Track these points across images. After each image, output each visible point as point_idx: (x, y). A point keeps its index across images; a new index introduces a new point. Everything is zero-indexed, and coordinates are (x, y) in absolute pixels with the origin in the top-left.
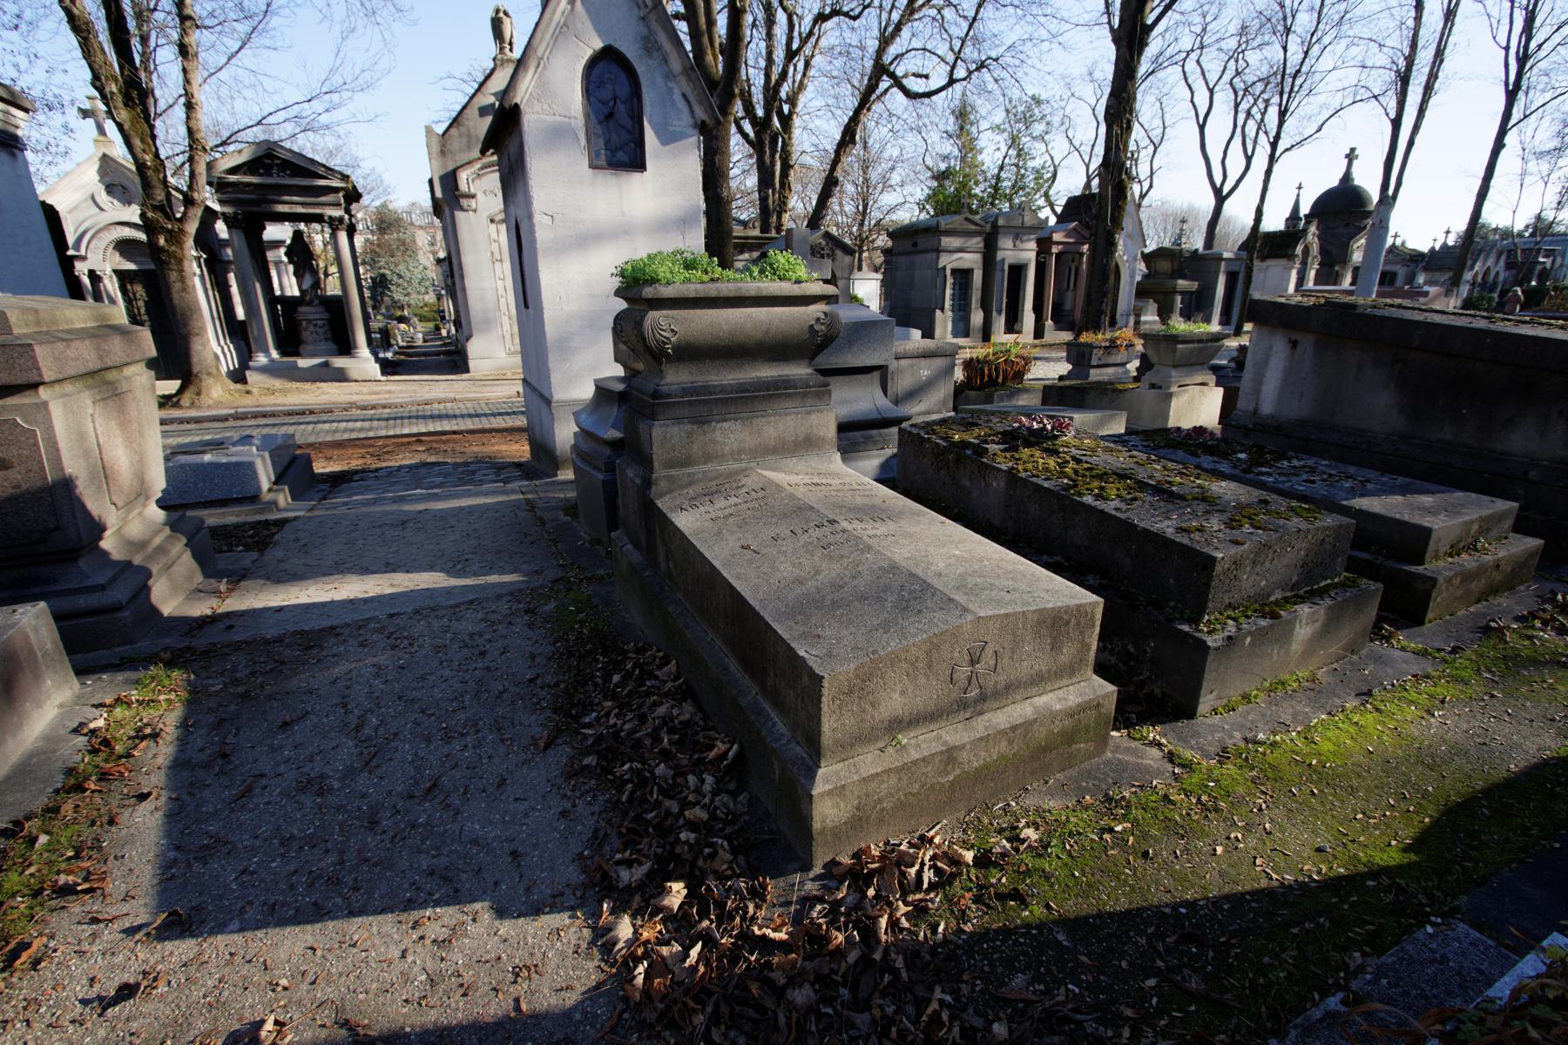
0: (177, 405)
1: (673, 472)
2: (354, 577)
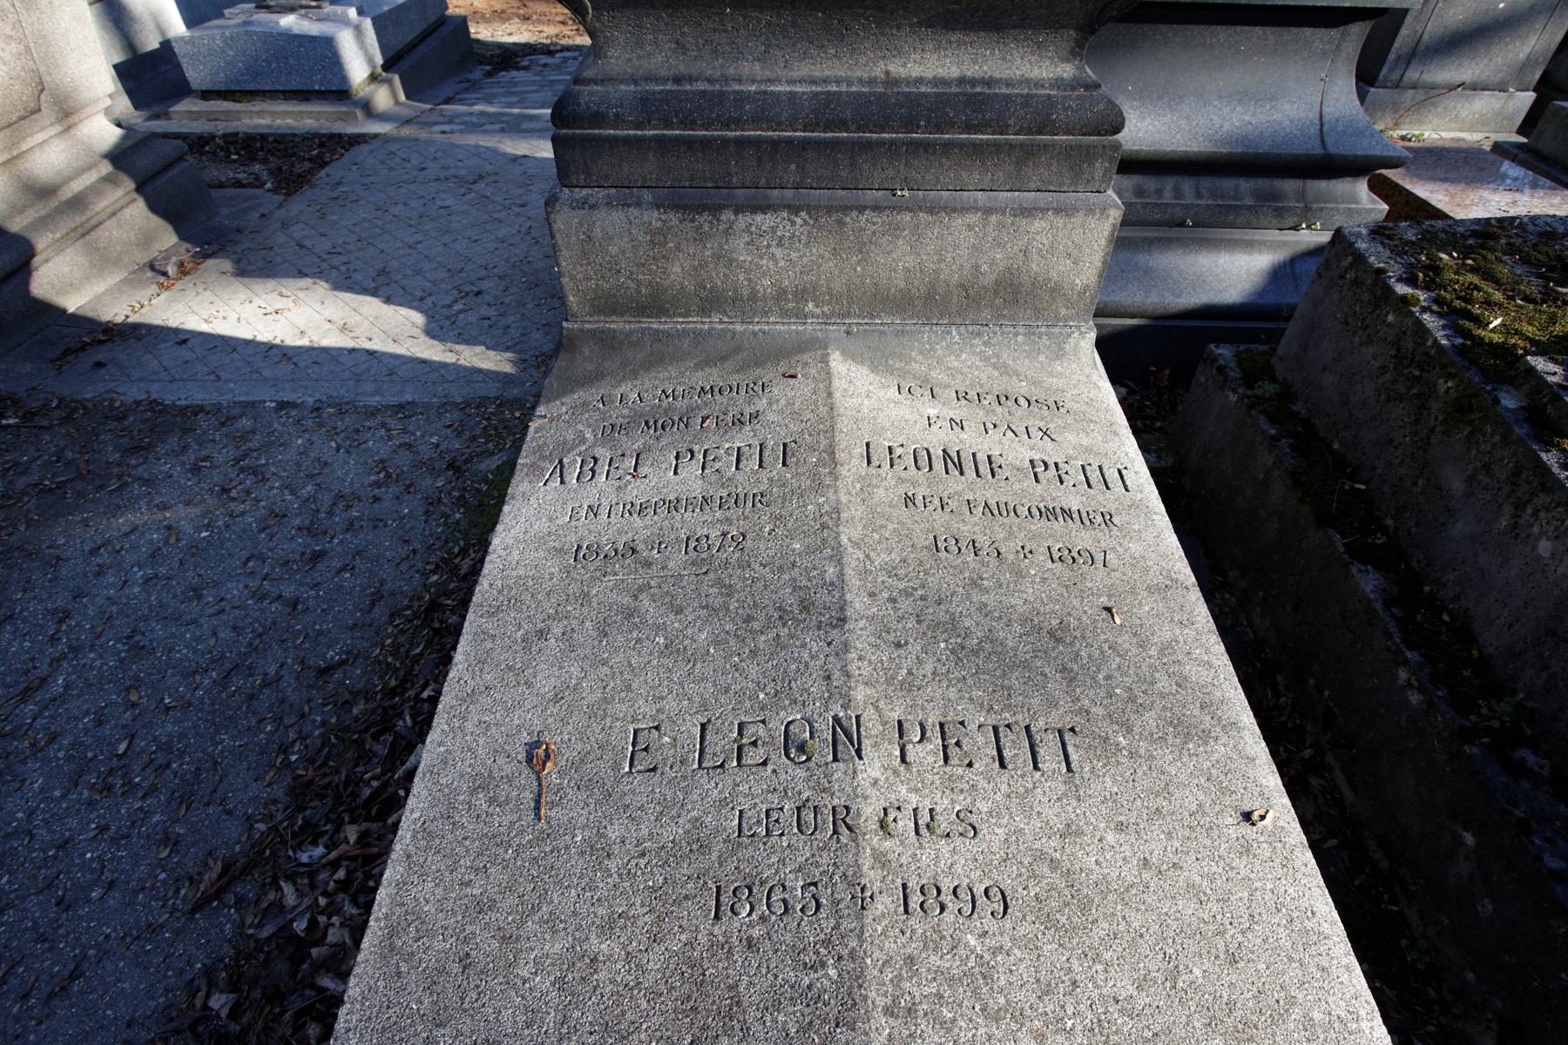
1: (617, 324)
2: (322, 287)
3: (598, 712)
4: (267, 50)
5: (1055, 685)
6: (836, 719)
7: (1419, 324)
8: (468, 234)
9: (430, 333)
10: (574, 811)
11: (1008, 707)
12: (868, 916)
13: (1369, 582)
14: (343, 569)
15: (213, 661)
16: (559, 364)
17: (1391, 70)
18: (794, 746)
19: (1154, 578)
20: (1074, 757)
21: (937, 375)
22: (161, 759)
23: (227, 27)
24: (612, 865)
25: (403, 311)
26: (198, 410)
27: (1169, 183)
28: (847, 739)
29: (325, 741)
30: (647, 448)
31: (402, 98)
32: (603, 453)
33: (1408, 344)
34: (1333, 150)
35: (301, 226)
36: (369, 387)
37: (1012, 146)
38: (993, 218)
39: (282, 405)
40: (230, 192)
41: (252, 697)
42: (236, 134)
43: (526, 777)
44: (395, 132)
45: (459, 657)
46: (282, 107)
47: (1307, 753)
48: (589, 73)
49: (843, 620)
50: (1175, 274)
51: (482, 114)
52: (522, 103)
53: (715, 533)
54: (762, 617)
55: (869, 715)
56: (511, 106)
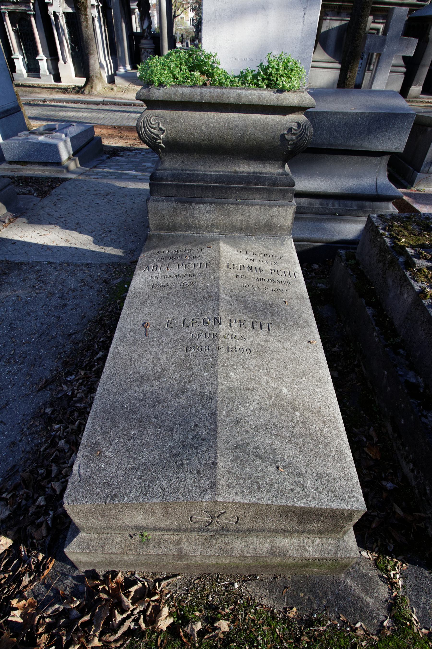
0: (83, 93)
1: (163, 233)
2: (58, 228)
3: (159, 317)
4: (34, 148)
5: (269, 315)
6: (215, 318)
7: (384, 241)
8: (106, 212)
9: (95, 243)
10: (154, 335)
11: (256, 318)
12: (220, 351)
13: (370, 311)
14: (73, 309)
15: (36, 332)
16: (147, 243)
17: (425, 167)
18: (205, 322)
19: (298, 296)
20: (270, 328)
21: (249, 248)
22: (24, 355)
23: (19, 140)
24: (163, 344)
25: (86, 236)
26: (22, 263)
27: (330, 202)
28: (217, 321)
29: (72, 352)
30: (171, 263)
31: (79, 165)
32: (159, 264)
33: (382, 246)
34: (379, 193)
35: (48, 208)
36: (77, 258)
37: (267, 189)
38: (263, 207)
39: (49, 263)
40: (22, 196)
41: (49, 341)
42: (22, 177)
43: (143, 329)
44: (78, 178)
45: (124, 307)
46: (37, 168)
47: (356, 363)
48: (160, 168)
49: (219, 299)
50: (333, 230)
51: (108, 172)
52: (121, 169)
53: (188, 282)
54: (199, 298)
55: (223, 318)
56: (118, 169)
